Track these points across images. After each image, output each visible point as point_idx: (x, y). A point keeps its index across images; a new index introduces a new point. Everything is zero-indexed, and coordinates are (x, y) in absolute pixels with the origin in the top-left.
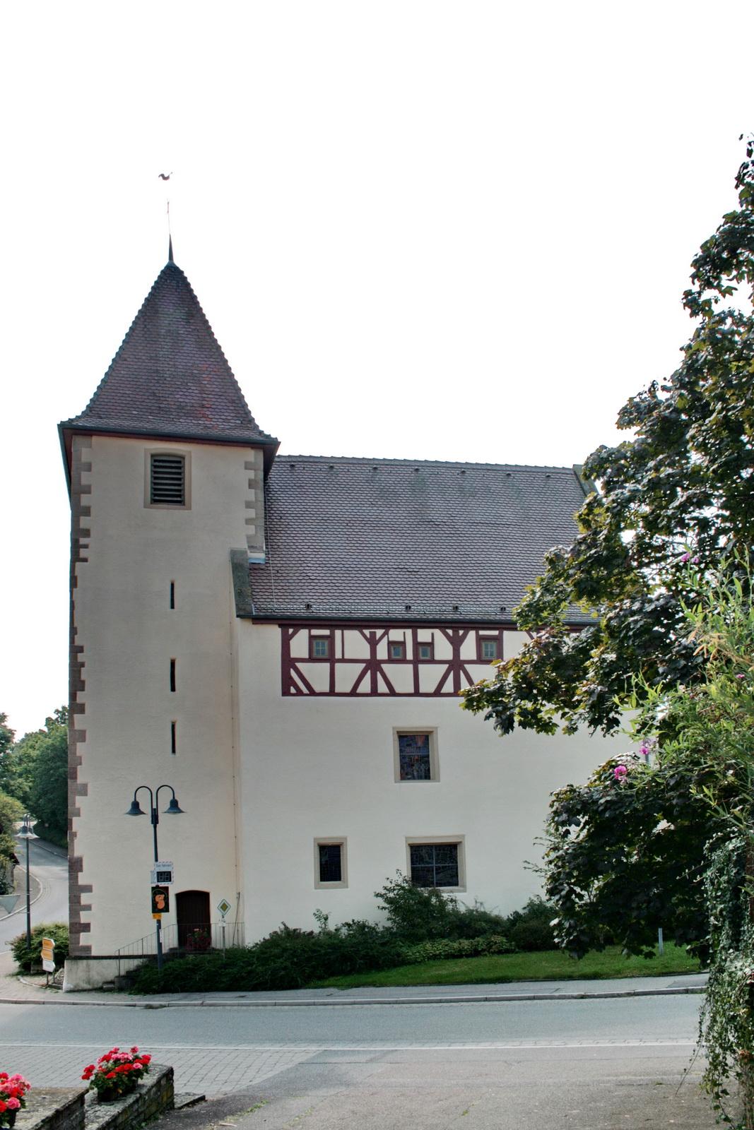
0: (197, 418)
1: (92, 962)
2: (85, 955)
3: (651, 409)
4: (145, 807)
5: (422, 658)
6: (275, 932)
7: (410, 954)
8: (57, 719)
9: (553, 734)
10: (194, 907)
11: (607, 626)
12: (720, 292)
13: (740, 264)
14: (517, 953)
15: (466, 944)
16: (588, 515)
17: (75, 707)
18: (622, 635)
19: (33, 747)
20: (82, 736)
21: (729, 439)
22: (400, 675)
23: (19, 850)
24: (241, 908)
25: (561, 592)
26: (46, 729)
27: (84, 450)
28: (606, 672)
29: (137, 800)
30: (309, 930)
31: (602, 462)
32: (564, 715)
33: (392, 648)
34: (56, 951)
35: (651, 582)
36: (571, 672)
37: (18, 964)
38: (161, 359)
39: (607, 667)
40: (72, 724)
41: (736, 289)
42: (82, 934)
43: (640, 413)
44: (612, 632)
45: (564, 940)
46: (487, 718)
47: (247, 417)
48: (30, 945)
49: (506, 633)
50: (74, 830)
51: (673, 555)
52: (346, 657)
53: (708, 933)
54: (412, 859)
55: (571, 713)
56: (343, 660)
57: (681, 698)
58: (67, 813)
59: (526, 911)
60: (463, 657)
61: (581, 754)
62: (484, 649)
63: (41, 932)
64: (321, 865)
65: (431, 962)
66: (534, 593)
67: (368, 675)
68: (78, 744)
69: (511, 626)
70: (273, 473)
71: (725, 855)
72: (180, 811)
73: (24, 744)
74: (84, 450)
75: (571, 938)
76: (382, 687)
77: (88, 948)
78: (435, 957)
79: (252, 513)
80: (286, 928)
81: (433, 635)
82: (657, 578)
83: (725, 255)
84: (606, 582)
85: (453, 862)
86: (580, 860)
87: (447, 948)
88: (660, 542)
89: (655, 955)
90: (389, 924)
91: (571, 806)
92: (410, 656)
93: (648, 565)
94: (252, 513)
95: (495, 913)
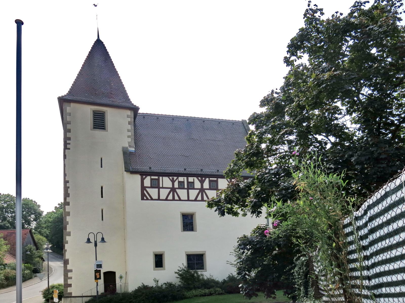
0: (109, 98)
1: (72, 298)
2: (70, 296)
3: (272, 100)
4: (92, 240)
5: (190, 187)
6: (140, 287)
7: (187, 294)
8: (59, 207)
9: (238, 217)
10: (110, 277)
11: (257, 178)
12: (297, 57)
13: (304, 47)
14: (225, 294)
15: (207, 291)
16: (250, 138)
17: (66, 203)
18: (262, 182)
19: (50, 217)
20: (68, 214)
21: (300, 111)
22: (183, 193)
23: (45, 256)
24: (127, 277)
25: (240, 165)
26: (55, 211)
27: (68, 108)
28: (257, 195)
29: (89, 238)
30: (151, 286)
31: (255, 119)
32: (242, 210)
33: (180, 184)
34: (59, 294)
35: (271, 163)
36: (244, 194)
37: (44, 299)
38: (96, 75)
39: (257, 192)
40: (65, 209)
41: (303, 57)
42: (68, 288)
43: (268, 102)
44: (260, 181)
45: (244, 292)
46: (216, 211)
47: (128, 98)
48: (49, 292)
49: (219, 180)
50: (66, 249)
51: (279, 153)
52: (163, 187)
53: (296, 291)
54: (187, 260)
55: (245, 209)
56: (163, 188)
57: (288, 206)
58: (63, 242)
59: (228, 279)
60: (205, 187)
61: (247, 223)
62: (211, 185)
63: (53, 287)
64: (156, 262)
65: (195, 297)
66: (230, 166)
67: (172, 193)
68: (67, 217)
69: (222, 177)
70: (137, 120)
71: (301, 262)
72: (105, 242)
73: (47, 216)
74: (68, 108)
75: (246, 292)
76: (176, 198)
77: (71, 293)
78: (196, 296)
79: (130, 134)
80: (144, 285)
81: (194, 179)
82: (274, 161)
83: (299, 44)
84: (256, 162)
85: (202, 261)
86: (248, 263)
87: (200, 293)
88: (274, 148)
89: (276, 298)
90: (180, 283)
91: (244, 243)
92: (186, 187)
93: (270, 156)
94: (130, 134)
95: (217, 280)
